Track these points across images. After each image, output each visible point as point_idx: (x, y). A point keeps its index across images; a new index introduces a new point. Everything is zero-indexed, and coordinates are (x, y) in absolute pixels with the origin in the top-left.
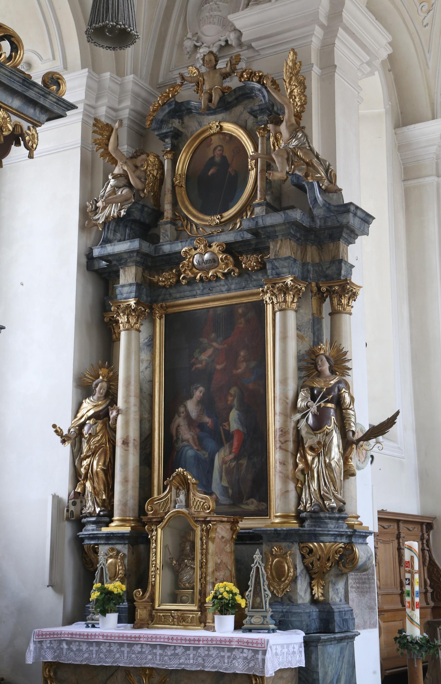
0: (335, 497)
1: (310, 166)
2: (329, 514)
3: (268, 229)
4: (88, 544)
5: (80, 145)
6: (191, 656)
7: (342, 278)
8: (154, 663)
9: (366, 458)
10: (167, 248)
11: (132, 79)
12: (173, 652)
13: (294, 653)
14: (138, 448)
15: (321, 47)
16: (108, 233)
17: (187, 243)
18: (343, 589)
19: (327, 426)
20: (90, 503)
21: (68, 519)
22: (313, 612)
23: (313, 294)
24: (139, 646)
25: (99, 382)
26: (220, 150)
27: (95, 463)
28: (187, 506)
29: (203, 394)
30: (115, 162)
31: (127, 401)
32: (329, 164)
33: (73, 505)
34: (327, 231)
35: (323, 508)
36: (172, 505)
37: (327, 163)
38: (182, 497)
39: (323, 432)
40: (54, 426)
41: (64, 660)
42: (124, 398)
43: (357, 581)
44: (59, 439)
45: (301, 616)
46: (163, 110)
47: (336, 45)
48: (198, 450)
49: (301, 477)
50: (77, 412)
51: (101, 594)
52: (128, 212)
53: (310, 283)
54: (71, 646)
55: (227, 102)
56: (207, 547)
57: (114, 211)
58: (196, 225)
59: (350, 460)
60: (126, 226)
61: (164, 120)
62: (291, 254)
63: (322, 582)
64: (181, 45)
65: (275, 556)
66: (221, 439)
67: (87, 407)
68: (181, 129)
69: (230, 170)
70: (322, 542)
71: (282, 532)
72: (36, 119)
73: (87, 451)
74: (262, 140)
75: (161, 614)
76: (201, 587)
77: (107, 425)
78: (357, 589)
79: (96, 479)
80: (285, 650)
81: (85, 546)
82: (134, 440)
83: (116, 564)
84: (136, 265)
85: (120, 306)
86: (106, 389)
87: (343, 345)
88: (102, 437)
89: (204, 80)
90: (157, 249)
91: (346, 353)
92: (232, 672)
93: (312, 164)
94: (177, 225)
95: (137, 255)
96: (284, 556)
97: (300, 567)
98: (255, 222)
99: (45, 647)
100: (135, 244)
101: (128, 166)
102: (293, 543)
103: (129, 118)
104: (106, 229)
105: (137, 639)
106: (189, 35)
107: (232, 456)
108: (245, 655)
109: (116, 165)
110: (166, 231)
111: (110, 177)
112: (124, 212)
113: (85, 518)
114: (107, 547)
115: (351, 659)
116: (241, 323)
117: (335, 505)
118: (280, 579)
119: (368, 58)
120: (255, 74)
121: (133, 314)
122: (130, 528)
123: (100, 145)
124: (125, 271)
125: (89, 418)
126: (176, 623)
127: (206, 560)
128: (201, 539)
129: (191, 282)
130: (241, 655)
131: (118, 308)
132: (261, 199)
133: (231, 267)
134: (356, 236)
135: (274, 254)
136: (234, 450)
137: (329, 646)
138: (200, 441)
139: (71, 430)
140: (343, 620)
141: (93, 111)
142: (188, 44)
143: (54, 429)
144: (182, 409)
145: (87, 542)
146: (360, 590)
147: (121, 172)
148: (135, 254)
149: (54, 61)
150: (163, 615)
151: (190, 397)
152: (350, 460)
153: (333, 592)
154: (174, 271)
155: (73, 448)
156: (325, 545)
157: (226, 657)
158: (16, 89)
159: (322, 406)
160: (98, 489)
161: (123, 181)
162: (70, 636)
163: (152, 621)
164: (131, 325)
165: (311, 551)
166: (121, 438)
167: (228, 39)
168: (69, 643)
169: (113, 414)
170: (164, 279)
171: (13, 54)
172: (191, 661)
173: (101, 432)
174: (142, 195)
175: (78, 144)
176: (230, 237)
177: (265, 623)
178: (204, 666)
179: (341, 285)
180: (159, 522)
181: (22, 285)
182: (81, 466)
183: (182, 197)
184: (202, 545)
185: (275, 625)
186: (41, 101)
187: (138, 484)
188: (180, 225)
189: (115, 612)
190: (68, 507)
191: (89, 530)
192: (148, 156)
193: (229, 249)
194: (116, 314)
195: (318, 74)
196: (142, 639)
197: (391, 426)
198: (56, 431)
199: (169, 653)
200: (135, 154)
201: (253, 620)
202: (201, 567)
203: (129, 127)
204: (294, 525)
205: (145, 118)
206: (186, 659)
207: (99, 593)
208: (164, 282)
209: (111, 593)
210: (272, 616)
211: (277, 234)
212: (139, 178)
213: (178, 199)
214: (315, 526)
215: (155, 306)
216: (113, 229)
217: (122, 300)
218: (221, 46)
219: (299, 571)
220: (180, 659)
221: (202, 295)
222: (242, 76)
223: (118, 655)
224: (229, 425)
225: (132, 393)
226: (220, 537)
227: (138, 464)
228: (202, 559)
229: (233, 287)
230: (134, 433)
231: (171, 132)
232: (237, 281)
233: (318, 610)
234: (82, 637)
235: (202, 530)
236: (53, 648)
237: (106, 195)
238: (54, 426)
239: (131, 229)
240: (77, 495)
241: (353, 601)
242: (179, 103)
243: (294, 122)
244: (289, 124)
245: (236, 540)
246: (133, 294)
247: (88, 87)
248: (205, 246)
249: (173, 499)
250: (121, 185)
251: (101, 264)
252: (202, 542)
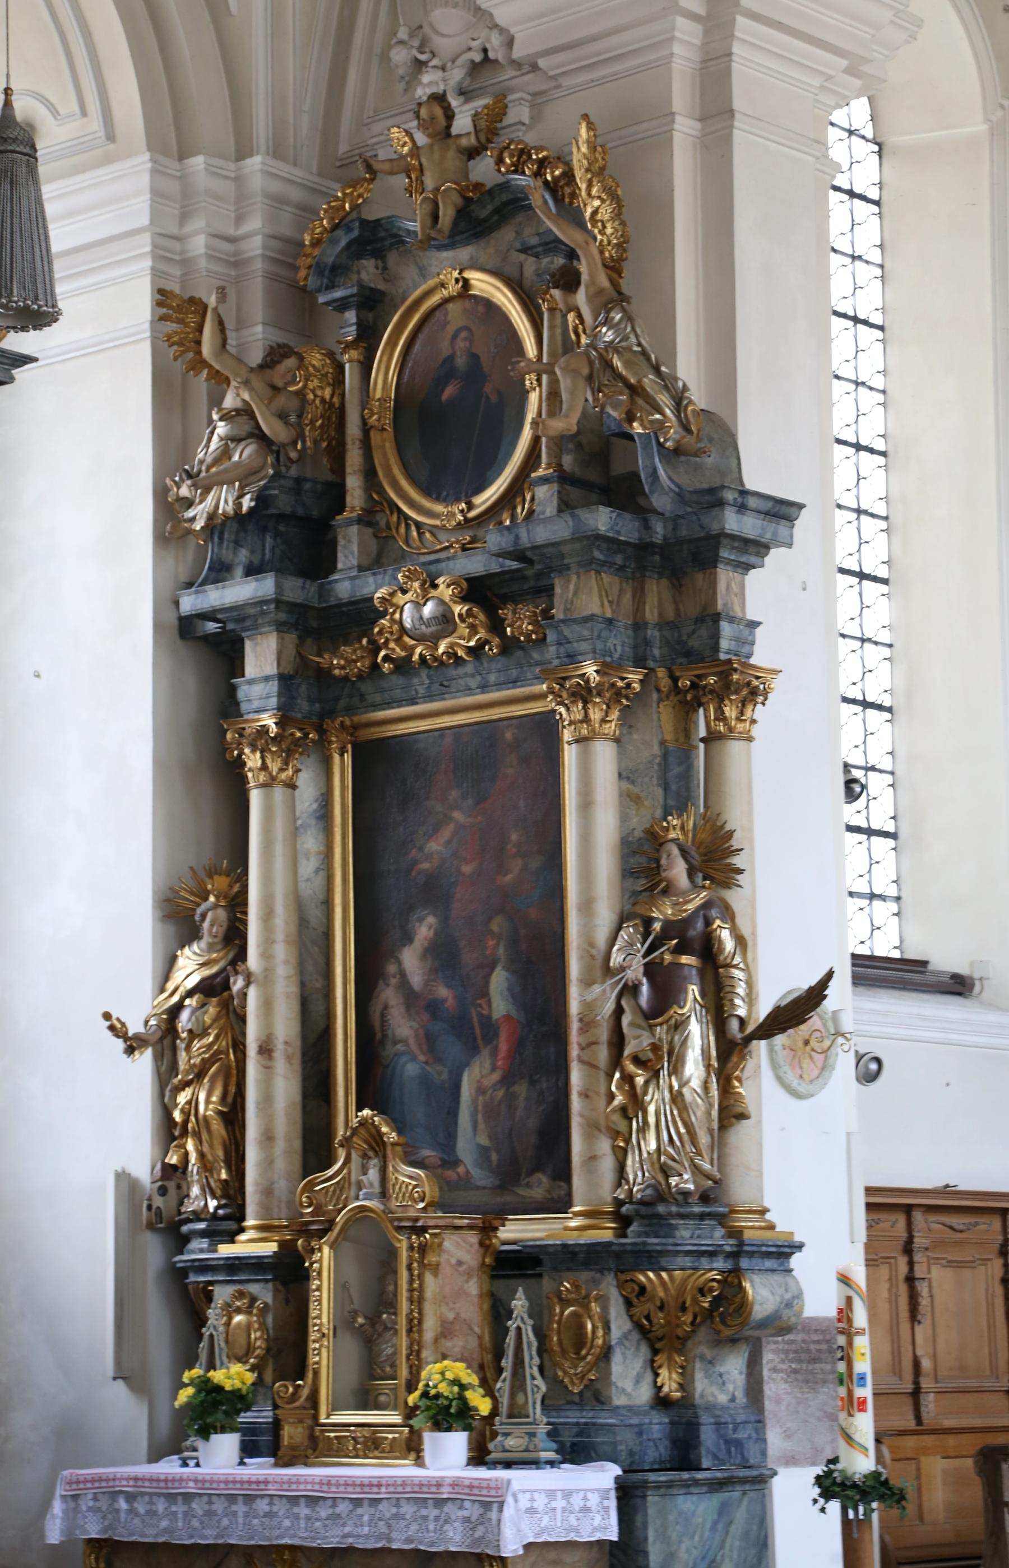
0: (696, 1169)
1: (638, 394)
2: (678, 1206)
3: (545, 551)
5: (148, 334)
6: (366, 1518)
7: (723, 656)
8: (295, 1536)
9: (823, 1069)
10: (344, 587)
11: (259, 167)
12: (330, 1511)
13: (585, 1510)
14: (297, 1060)
15: (703, 62)
17: (387, 578)
18: (741, 1373)
19: (675, 1008)
20: (195, 1190)
21: (151, 1226)
22: (651, 1423)
23: (663, 695)
24: (266, 1500)
26: (465, 339)
27: (202, 1096)
28: (384, 1195)
29: (436, 934)
30: (220, 381)
31: (266, 955)
32: (684, 385)
34: (685, 547)
35: (660, 1195)
36: (353, 1193)
37: (680, 384)
38: (373, 1174)
39: (667, 1021)
40: (107, 1016)
41: (122, 1535)
43: (791, 1356)
44: (120, 1044)
45: (614, 1433)
46: (333, 242)
47: (734, 58)
48: (426, 1063)
49: (621, 1125)
50: (166, 978)
51: (199, 1391)
52: (262, 500)
53: (652, 670)
54: (136, 1505)
55: (480, 217)
56: (421, 1285)
57: (226, 502)
58: (418, 525)
59: (737, 1084)
60: (264, 530)
61: (342, 262)
62: (602, 605)
63: (679, 1359)
64: (385, 57)
65: (565, 1303)
66: (475, 1039)
68: (381, 286)
69: (488, 389)
70: (665, 1270)
71: (577, 1249)
74: (551, 319)
75: (332, 1435)
76: (411, 1373)
78: (793, 1376)
80: (559, 1503)
81: (190, 1287)
83: (249, 1326)
84: (278, 631)
86: (225, 925)
87: (724, 817)
88: (217, 1037)
89: (421, 165)
90: (324, 592)
91: (730, 834)
92: (441, 1549)
93: (644, 389)
94: (377, 524)
95: (277, 608)
96: (584, 1302)
97: (620, 1324)
98: (512, 537)
99: (84, 1508)
100: (264, 587)
102: (602, 1273)
104: (216, 540)
105: (262, 1486)
106: (403, 34)
107: (496, 1077)
108: (466, 1513)
110: (350, 547)
111: (215, 417)
115: (755, 1528)
116: (510, 768)
117: (691, 1186)
118: (578, 1353)
119: (844, 63)
120: (530, 156)
121: (274, 749)
123: (183, 345)
125: (190, 994)
126: (361, 1453)
127: (420, 1313)
128: (409, 1268)
129: (403, 666)
130: (460, 1513)
131: (241, 735)
132: (549, 466)
133: (482, 634)
134: (762, 550)
135: (562, 607)
136: (500, 1063)
137: (681, 1498)
138: (429, 1041)
140: (728, 1442)
141: (176, 246)
142: (400, 56)
143: (108, 1023)
144: (391, 968)
145: (193, 1278)
146: (799, 1377)
147: (239, 404)
148: (272, 606)
149: (85, 120)
150: (336, 1437)
151: (408, 938)
152: (737, 1084)
153: (706, 1381)
154: (364, 641)
156: (671, 1277)
157: (431, 1518)
159: (666, 963)
160: (210, 1157)
161: (245, 426)
162: (131, 1483)
163: (314, 1450)
164: (270, 774)
165: (643, 1290)
166: (258, 1040)
167: (488, 46)
168: (130, 1498)
169: (237, 984)
170: (342, 662)
172: (366, 1530)
175: (144, 331)
176: (476, 565)
177: (531, 1447)
178: (390, 1540)
179: (721, 672)
180: (324, 1232)
181: (38, 676)
183: (385, 455)
184: (411, 1281)
185: (557, 1452)
187: (298, 1144)
188: (383, 524)
189: (233, 1430)
190: (149, 1199)
191: (193, 1252)
193: (477, 591)
195: (695, 133)
196: (270, 1486)
197: (818, 1004)
198: (112, 1028)
199: (324, 1514)
201: (511, 1442)
202: (410, 1331)
203: (270, 277)
204: (605, 1234)
206: (356, 1526)
208: (343, 668)
209: (219, 1389)
210: (549, 1434)
211: (566, 562)
212: (282, 416)
213: (377, 462)
214: (647, 1234)
215: (327, 724)
216: (233, 537)
218: (473, 61)
219: (615, 1334)
220: (343, 1525)
221: (430, 698)
222: (500, 161)
223: (225, 1522)
224: (489, 1004)
225: (280, 935)
226: (453, 1261)
227: (297, 1097)
228: (412, 1311)
229: (492, 678)
230: (286, 1026)
231: (353, 296)
232: (499, 666)
233: (667, 1420)
234: (140, 1483)
235: (411, 1248)
236: (99, 1510)
237: (209, 460)
238: (107, 1016)
239: (277, 534)
241: (778, 1402)
242: (369, 222)
243: (605, 283)
244: (592, 290)
245: (493, 1268)
246: (273, 702)
247: (157, 195)
248: (422, 585)
249: (353, 1178)
250: (243, 434)
252: (411, 1275)
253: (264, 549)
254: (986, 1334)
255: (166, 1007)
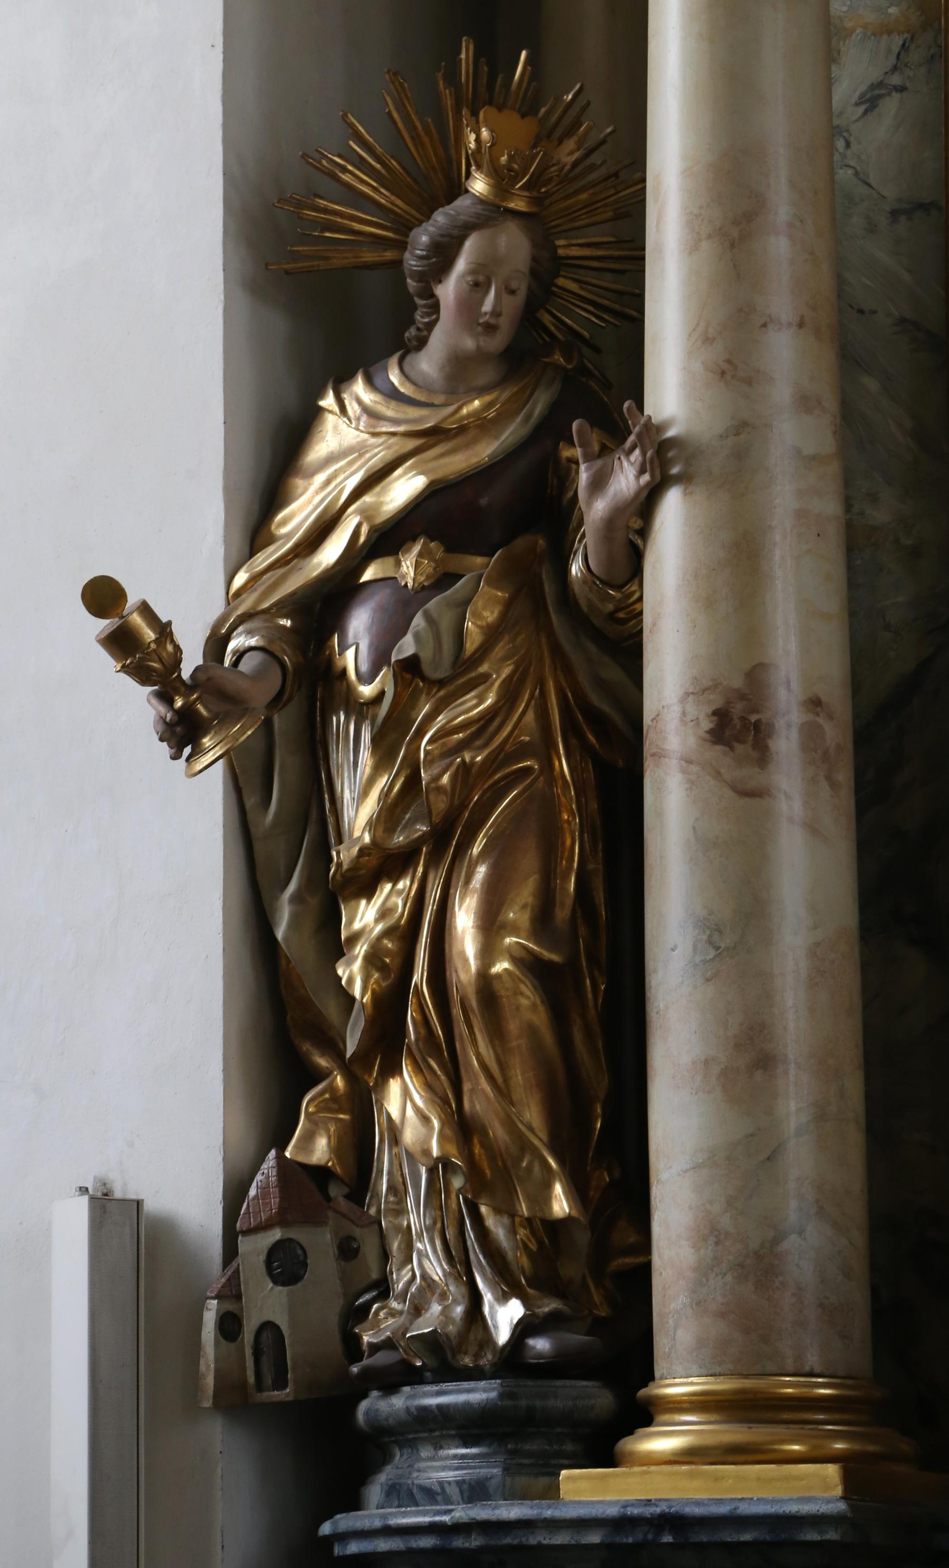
14: (845, 775)
21: (234, 1400)
27: (465, 920)
31: (731, 364)
33: (277, 1280)
40: (102, 596)
44: (138, 705)
67: (359, 450)
77: (549, 589)
79: (477, 1051)
88: (509, 697)
113: (390, 1389)
122: (832, 1471)
125: (387, 539)
139: (232, 645)
143: (102, 625)
160: (498, 1132)
173: (500, 650)
182: (337, 949)
190: (232, 1291)
198: (121, 643)
225: (781, 303)
227: (843, 909)
238: (102, 596)
240: (305, 1190)
254: (577, 1499)
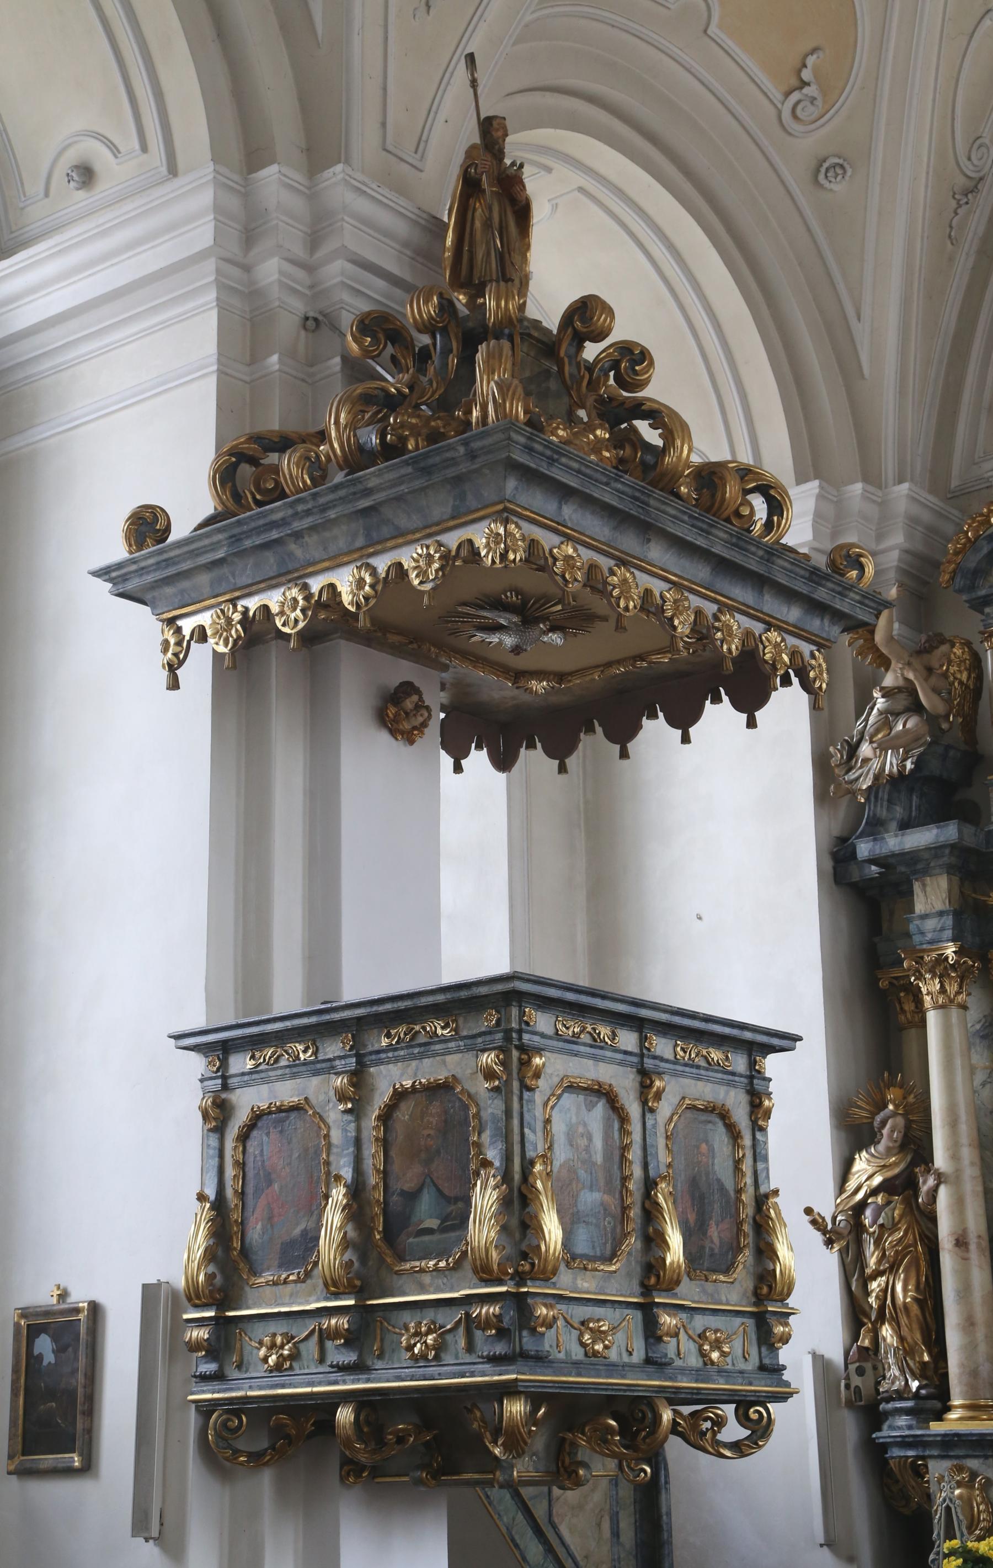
4: (901, 1457)
11: (906, 492)
14: (987, 1253)
16: (875, 806)
20: (894, 1371)
21: (850, 1404)
25: (889, 1118)
27: (899, 1287)
30: (885, 663)
31: (955, 1156)
40: (808, 1211)
42: (948, 1149)
44: (818, 1237)
51: (965, 1562)
57: (891, 764)
60: (911, 791)
72: (824, 635)
73: (879, 1262)
77: (914, 1205)
79: (904, 1320)
81: (891, 1462)
82: (979, 1237)
84: (948, 873)
85: (922, 958)
95: (951, 852)
100: (950, 832)
101: (915, 670)
103: (900, 570)
104: (873, 799)
109: (887, 670)
111: (877, 694)
112: (912, 763)
114: (947, 1464)
121: (953, 975)
124: (924, 885)
125: (874, 1192)
147: (901, 683)
148: (947, 851)
155: (844, 1256)
158: (800, 590)
160: (909, 1340)
161: (902, 701)
164: (949, 997)
171: (775, 518)
173: (903, 1222)
174: (945, 726)
175: (212, 365)
181: (700, 918)
182: (868, 1294)
186: (838, 605)
190: (848, 1378)
192: (953, 646)
194: (914, 975)
198: (814, 1222)
200: (927, 645)
205: (939, 568)
207: (961, 1560)
216: (886, 797)
217: (924, 946)
238: (808, 1211)
246: (948, 933)
251: (867, 871)
253: (911, 807)
255: (852, 1203)
